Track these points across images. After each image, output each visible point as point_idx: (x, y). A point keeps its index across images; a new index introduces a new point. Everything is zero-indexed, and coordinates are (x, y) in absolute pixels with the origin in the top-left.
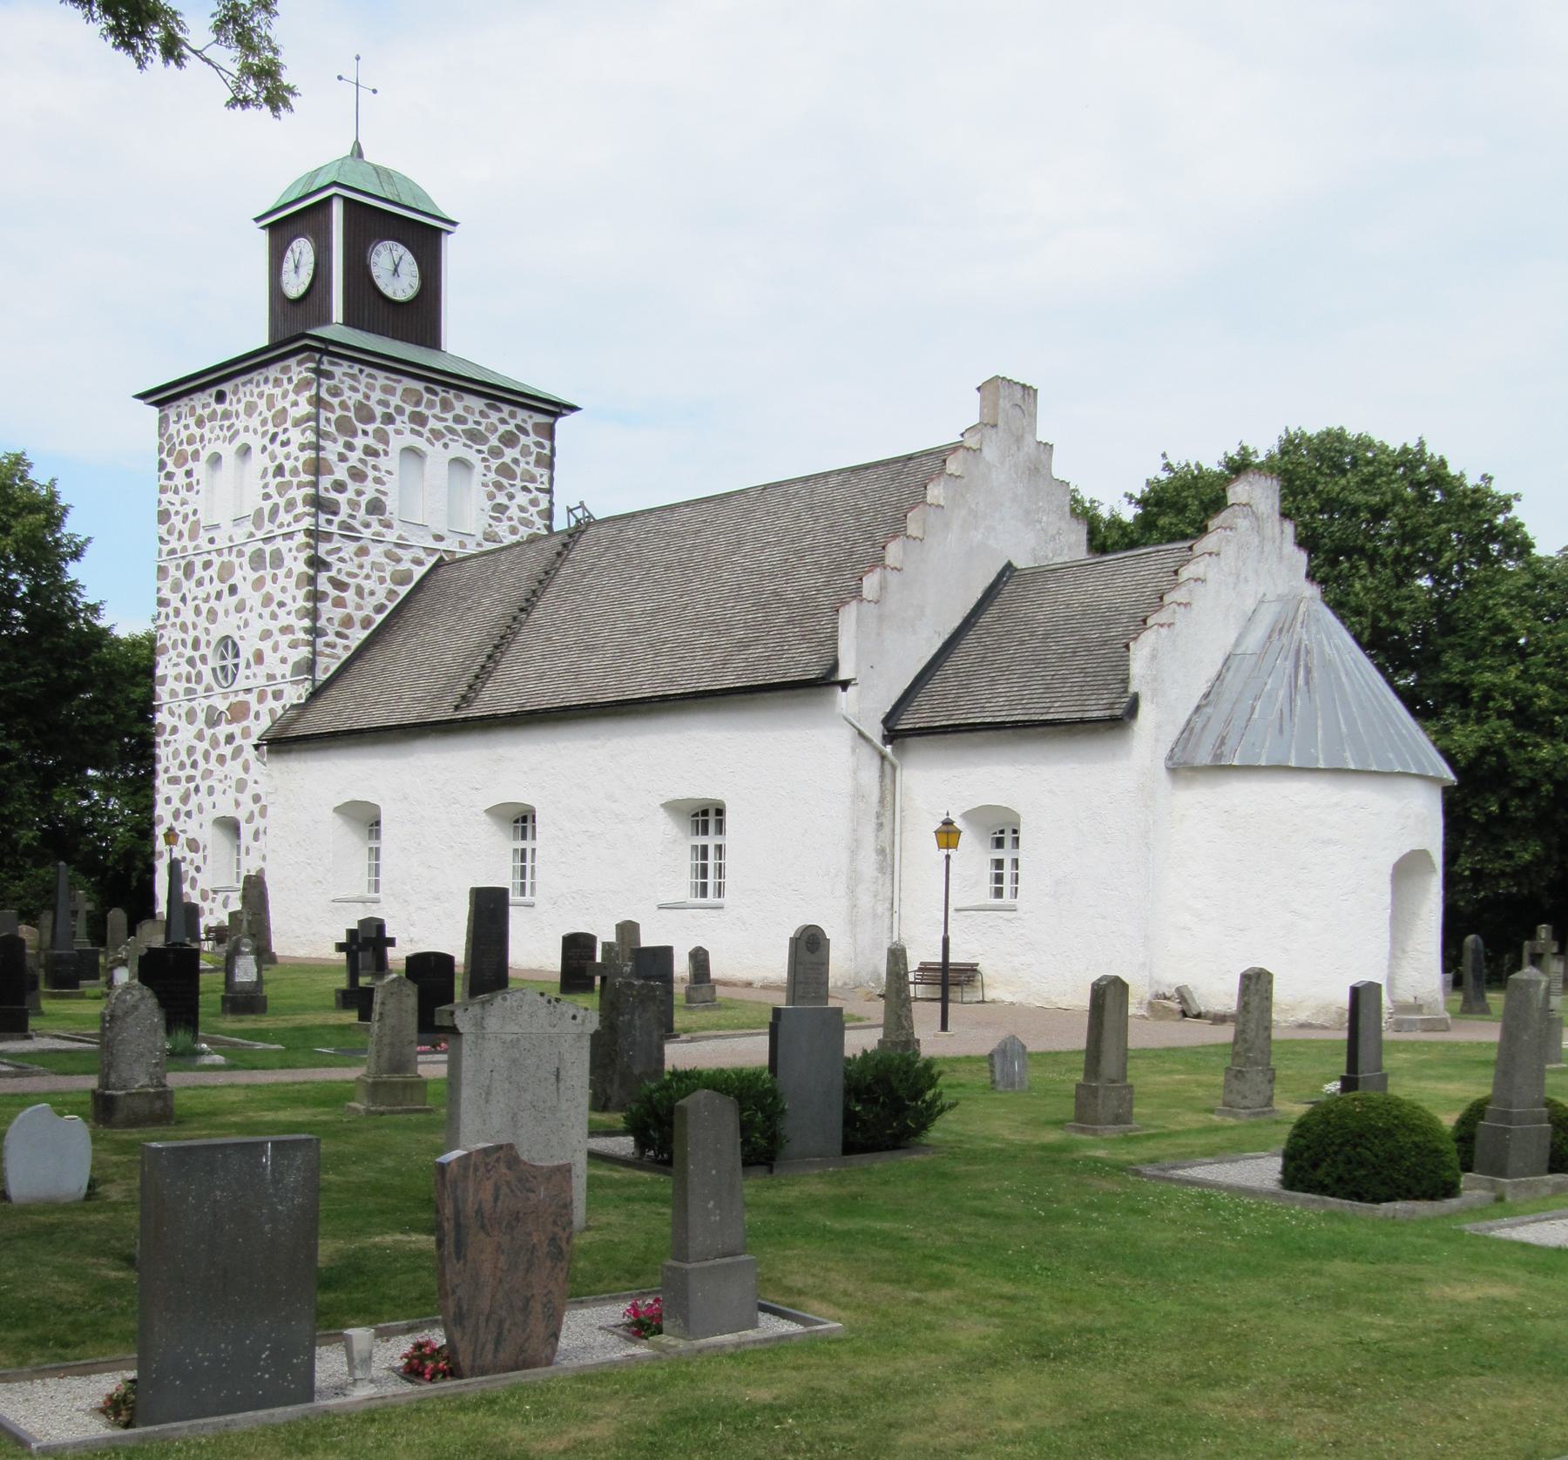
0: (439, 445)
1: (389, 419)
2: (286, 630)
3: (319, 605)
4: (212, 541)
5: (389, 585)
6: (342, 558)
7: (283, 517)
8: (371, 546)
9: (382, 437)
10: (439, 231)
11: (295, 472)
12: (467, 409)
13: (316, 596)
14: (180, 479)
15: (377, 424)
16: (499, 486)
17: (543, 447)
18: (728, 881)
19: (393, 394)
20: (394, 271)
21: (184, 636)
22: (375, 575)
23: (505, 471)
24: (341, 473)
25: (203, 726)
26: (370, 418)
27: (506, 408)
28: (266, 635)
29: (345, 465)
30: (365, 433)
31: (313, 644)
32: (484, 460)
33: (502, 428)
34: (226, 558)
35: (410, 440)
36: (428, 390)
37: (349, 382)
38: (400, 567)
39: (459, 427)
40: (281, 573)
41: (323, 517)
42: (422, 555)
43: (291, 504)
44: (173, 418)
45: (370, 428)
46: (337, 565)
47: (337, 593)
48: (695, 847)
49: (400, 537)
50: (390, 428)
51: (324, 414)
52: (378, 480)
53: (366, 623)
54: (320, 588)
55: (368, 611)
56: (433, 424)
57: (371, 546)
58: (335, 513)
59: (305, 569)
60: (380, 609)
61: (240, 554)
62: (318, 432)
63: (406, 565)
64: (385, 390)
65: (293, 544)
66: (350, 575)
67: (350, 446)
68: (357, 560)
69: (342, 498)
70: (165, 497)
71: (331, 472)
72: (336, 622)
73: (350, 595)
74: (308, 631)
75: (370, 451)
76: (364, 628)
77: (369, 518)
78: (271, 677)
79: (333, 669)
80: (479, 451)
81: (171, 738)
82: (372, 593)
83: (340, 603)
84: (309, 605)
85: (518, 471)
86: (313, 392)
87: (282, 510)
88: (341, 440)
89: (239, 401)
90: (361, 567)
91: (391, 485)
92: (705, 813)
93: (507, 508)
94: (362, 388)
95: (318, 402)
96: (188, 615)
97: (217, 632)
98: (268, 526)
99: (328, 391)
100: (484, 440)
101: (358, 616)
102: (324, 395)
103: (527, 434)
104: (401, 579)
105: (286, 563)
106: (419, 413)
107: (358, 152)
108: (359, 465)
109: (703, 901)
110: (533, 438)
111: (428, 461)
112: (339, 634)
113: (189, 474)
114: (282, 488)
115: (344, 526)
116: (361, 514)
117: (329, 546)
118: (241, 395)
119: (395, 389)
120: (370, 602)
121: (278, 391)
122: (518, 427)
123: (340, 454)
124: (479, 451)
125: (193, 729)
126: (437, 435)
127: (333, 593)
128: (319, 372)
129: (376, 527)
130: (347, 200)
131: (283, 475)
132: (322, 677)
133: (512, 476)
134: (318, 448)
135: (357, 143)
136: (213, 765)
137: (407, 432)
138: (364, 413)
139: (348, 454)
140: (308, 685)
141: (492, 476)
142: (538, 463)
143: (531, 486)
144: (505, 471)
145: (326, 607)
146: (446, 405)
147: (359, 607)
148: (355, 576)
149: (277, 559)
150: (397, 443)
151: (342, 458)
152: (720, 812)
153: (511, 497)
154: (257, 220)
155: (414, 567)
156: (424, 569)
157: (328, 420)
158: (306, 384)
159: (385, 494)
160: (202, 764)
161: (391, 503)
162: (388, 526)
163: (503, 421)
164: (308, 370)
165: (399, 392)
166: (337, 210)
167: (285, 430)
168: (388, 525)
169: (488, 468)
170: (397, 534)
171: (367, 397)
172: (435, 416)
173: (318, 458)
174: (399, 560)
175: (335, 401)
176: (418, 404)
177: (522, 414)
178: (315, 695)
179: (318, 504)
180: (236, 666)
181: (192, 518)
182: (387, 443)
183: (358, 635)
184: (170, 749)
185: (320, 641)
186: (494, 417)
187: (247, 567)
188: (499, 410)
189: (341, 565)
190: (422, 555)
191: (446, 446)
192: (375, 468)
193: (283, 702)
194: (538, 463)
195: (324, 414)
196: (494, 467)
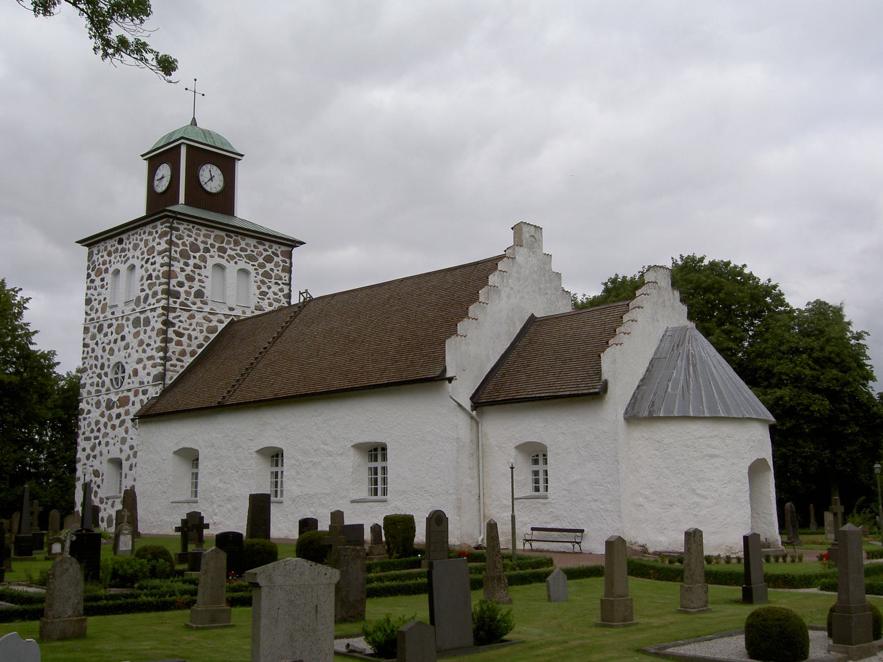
0: (232, 262)
1: (207, 250)
2: (150, 358)
5: (205, 333)
6: (181, 319)
7: (151, 300)
8: (196, 314)
9: (203, 259)
11: (158, 278)
12: (247, 244)
13: (167, 340)
14: (98, 282)
15: (201, 253)
16: (263, 282)
18: (390, 487)
23: (266, 275)
24: (181, 277)
25: (104, 409)
27: (267, 244)
28: (140, 361)
29: (184, 274)
30: (195, 257)
31: (164, 365)
32: (256, 269)
33: (265, 254)
34: (120, 322)
36: (227, 235)
37: (187, 232)
39: (243, 254)
40: (149, 329)
41: (171, 300)
42: (223, 318)
43: (155, 294)
44: (95, 252)
45: (197, 255)
50: (207, 255)
51: (173, 248)
52: (200, 281)
53: (193, 353)
54: (169, 336)
55: (194, 347)
56: (229, 252)
57: (196, 314)
59: (162, 326)
61: (128, 320)
62: (170, 257)
64: (205, 236)
65: (156, 314)
66: (184, 329)
67: (187, 264)
68: (188, 322)
69: (182, 290)
70: (89, 292)
71: (177, 277)
72: (177, 354)
73: (184, 340)
74: (161, 358)
75: (196, 266)
76: (192, 356)
78: (142, 383)
79: (175, 378)
82: (196, 338)
83: (179, 343)
84: (163, 345)
85: (273, 275)
86: (168, 237)
88: (182, 261)
89: (130, 243)
90: (191, 325)
91: (208, 283)
92: (376, 450)
94: (194, 236)
95: (170, 243)
97: (114, 360)
98: (142, 305)
101: (188, 350)
102: (174, 239)
107: (194, 122)
108: (191, 274)
110: (281, 258)
111: (227, 270)
112: (178, 360)
113: (102, 280)
114: (151, 286)
115: (182, 304)
116: (192, 298)
117: (174, 315)
120: (195, 343)
121: (151, 238)
122: (273, 252)
125: (99, 411)
126: (232, 257)
127: (176, 338)
129: (199, 304)
130: (188, 146)
132: (168, 382)
136: (109, 430)
140: (161, 386)
141: (260, 277)
142: (283, 271)
143: (280, 282)
144: (266, 275)
145: (172, 346)
146: (237, 243)
147: (189, 346)
148: (188, 329)
149: (147, 322)
150: (210, 262)
151: (182, 270)
153: (269, 288)
154: (142, 156)
155: (218, 324)
156: (224, 325)
157: (176, 251)
160: (103, 430)
161: (207, 292)
163: (265, 250)
164: (166, 227)
165: (212, 237)
166: (183, 151)
168: (206, 303)
169: (257, 274)
171: (196, 240)
174: (210, 321)
175: (180, 242)
176: (222, 243)
177: (275, 246)
178: (164, 392)
179: (169, 293)
180: (123, 377)
181: (103, 302)
183: (188, 360)
184: (86, 422)
185: (168, 364)
186: (261, 248)
189: (180, 324)
190: (223, 318)
191: (236, 263)
192: (199, 275)
194: (283, 271)
195: (173, 248)
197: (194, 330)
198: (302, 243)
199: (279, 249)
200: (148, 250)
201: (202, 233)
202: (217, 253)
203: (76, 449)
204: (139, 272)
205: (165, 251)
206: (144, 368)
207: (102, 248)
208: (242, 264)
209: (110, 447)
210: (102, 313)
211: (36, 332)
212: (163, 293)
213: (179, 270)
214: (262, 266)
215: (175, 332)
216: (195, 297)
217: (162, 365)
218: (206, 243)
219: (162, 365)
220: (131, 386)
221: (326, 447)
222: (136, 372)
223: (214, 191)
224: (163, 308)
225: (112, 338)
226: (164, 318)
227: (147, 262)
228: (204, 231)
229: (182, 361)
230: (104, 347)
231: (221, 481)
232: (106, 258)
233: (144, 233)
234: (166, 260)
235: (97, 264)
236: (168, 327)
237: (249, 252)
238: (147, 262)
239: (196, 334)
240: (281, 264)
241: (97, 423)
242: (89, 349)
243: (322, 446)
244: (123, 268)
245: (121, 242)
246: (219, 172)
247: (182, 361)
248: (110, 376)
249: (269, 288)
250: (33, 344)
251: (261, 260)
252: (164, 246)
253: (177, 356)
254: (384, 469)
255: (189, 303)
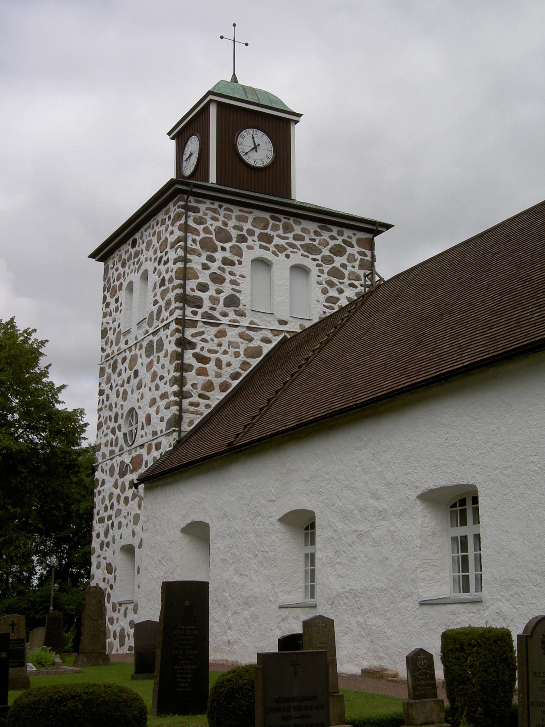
0: (282, 256)
1: (242, 239)
2: (164, 396)
3: (185, 374)
4: (127, 343)
5: (242, 358)
6: (205, 339)
7: (165, 314)
8: (228, 330)
9: (238, 252)
10: (289, 121)
11: (171, 280)
12: (303, 230)
13: (182, 368)
14: (113, 306)
15: (234, 242)
16: (331, 284)
17: (366, 256)
18: (486, 574)
19: (246, 222)
20: (254, 147)
21: (110, 413)
22: (232, 350)
23: (336, 273)
24: (204, 277)
25: (118, 477)
26: (229, 239)
27: (335, 229)
28: (153, 402)
29: (207, 272)
30: (223, 249)
31: (179, 404)
32: (318, 265)
33: (332, 243)
34: (133, 353)
35: (259, 253)
36: (273, 218)
37: (210, 214)
38: (251, 345)
39: (298, 243)
40: (162, 354)
41: (189, 310)
42: (270, 335)
43: (168, 303)
44: (111, 266)
45: (228, 246)
46: (200, 345)
47: (201, 365)
48: (454, 539)
49: (252, 322)
50: (243, 246)
51: (190, 236)
52: (233, 282)
53: (224, 387)
54: (186, 361)
55: (226, 378)
56: (277, 241)
57: (228, 330)
58: (200, 307)
59: (175, 348)
60: (235, 376)
61: (141, 347)
62: (186, 249)
63: (256, 343)
64: (238, 218)
65: (168, 332)
66: (210, 351)
67: (212, 259)
68: (216, 341)
69: (205, 296)
70: (105, 320)
71: (197, 277)
72: (199, 387)
73: (211, 367)
74: (175, 394)
75: (226, 261)
76: (223, 391)
77: (226, 309)
78: (155, 433)
79: (196, 422)
80: (314, 260)
81: (101, 489)
82: (229, 364)
83: (202, 372)
84: (178, 374)
85: (346, 273)
86: (183, 221)
87: (163, 309)
88: (204, 254)
89: (143, 243)
90: (220, 345)
91: (245, 285)
92: (463, 502)
93: (338, 299)
94: (221, 218)
95: (186, 228)
96: (113, 396)
97: (127, 406)
98: (156, 323)
99: (195, 221)
100: (319, 252)
101: (217, 382)
102: (191, 223)
103: (352, 246)
104: (253, 353)
105: (165, 347)
106: (266, 234)
107: (234, 79)
108: (219, 272)
109: (465, 596)
110: (357, 248)
111: (274, 267)
112: (201, 396)
113: (117, 301)
114: (164, 294)
115: (206, 315)
116: (220, 307)
117: (194, 331)
118: (144, 238)
119: (247, 218)
120: (227, 372)
121: (163, 228)
122: (344, 241)
123: (203, 264)
124: (314, 260)
125: (113, 480)
126: (280, 249)
127: (197, 365)
128: (187, 208)
129: (232, 315)
130: (220, 105)
131: (164, 285)
132: (186, 428)
133: (341, 276)
134: (185, 260)
135: (234, 75)
136: (122, 506)
137: (257, 247)
138: (223, 235)
139: (210, 264)
140: (175, 435)
141: (325, 277)
142: (361, 267)
143: (356, 283)
144: (336, 273)
145: (191, 376)
146: (287, 229)
147: (218, 375)
148: (216, 352)
149: (160, 344)
150: (248, 256)
151: (205, 267)
152: (475, 500)
153: (341, 291)
155: (263, 344)
156: (271, 346)
157: (194, 241)
158: (178, 217)
159: (239, 292)
160: (116, 506)
161: (244, 298)
162: (243, 315)
163: (333, 238)
164: (179, 207)
165: (250, 220)
167: (167, 253)
168: (242, 314)
169: (322, 271)
170: (249, 320)
171: (226, 224)
172: (279, 236)
173: (185, 267)
174: (251, 340)
175: (200, 228)
176: (265, 228)
177: (347, 233)
178: (179, 443)
179: (185, 299)
180: (136, 429)
181: (117, 330)
182: (241, 255)
183: (217, 397)
184: (101, 497)
185: (186, 402)
186: (326, 235)
187: (144, 355)
188: (330, 230)
189: (204, 344)
190: (270, 335)
191: (288, 256)
192: (231, 273)
193: (161, 451)
194: (361, 267)
195: (190, 236)
196: (326, 270)
197: (225, 352)
198: (388, 227)
199: (355, 237)
200: (161, 246)
201: (233, 215)
202: (258, 243)
203: (91, 536)
204: (154, 278)
205: (178, 240)
206: (157, 412)
207: (117, 258)
208: (297, 258)
209: (123, 530)
210: (117, 345)
211: (63, 387)
212: (176, 300)
213: (200, 267)
214: (328, 260)
215: (195, 355)
216: (226, 305)
217: (176, 403)
218: (240, 229)
219: (176, 403)
220: (145, 439)
221: (376, 503)
222: (148, 419)
223: (260, 164)
224: (177, 321)
225: (125, 376)
226: (178, 335)
227: (159, 263)
228: (236, 211)
229: (208, 398)
230: (118, 391)
231: (237, 571)
232: (121, 270)
233: (157, 224)
234: (180, 252)
235: (112, 280)
236: (184, 349)
237: (307, 241)
238: (159, 263)
239: (227, 358)
240: (357, 256)
241: (111, 496)
242: (104, 397)
243: (371, 501)
244: (135, 278)
245: (134, 245)
246: (266, 138)
247: (208, 398)
248: (124, 430)
249: (341, 291)
250: (59, 402)
251: (326, 252)
252: (178, 233)
253: (199, 391)
254: (477, 537)
255: (216, 314)
